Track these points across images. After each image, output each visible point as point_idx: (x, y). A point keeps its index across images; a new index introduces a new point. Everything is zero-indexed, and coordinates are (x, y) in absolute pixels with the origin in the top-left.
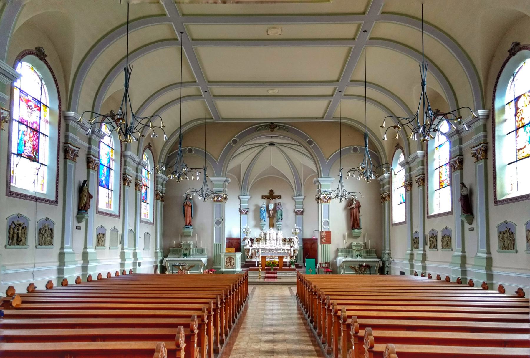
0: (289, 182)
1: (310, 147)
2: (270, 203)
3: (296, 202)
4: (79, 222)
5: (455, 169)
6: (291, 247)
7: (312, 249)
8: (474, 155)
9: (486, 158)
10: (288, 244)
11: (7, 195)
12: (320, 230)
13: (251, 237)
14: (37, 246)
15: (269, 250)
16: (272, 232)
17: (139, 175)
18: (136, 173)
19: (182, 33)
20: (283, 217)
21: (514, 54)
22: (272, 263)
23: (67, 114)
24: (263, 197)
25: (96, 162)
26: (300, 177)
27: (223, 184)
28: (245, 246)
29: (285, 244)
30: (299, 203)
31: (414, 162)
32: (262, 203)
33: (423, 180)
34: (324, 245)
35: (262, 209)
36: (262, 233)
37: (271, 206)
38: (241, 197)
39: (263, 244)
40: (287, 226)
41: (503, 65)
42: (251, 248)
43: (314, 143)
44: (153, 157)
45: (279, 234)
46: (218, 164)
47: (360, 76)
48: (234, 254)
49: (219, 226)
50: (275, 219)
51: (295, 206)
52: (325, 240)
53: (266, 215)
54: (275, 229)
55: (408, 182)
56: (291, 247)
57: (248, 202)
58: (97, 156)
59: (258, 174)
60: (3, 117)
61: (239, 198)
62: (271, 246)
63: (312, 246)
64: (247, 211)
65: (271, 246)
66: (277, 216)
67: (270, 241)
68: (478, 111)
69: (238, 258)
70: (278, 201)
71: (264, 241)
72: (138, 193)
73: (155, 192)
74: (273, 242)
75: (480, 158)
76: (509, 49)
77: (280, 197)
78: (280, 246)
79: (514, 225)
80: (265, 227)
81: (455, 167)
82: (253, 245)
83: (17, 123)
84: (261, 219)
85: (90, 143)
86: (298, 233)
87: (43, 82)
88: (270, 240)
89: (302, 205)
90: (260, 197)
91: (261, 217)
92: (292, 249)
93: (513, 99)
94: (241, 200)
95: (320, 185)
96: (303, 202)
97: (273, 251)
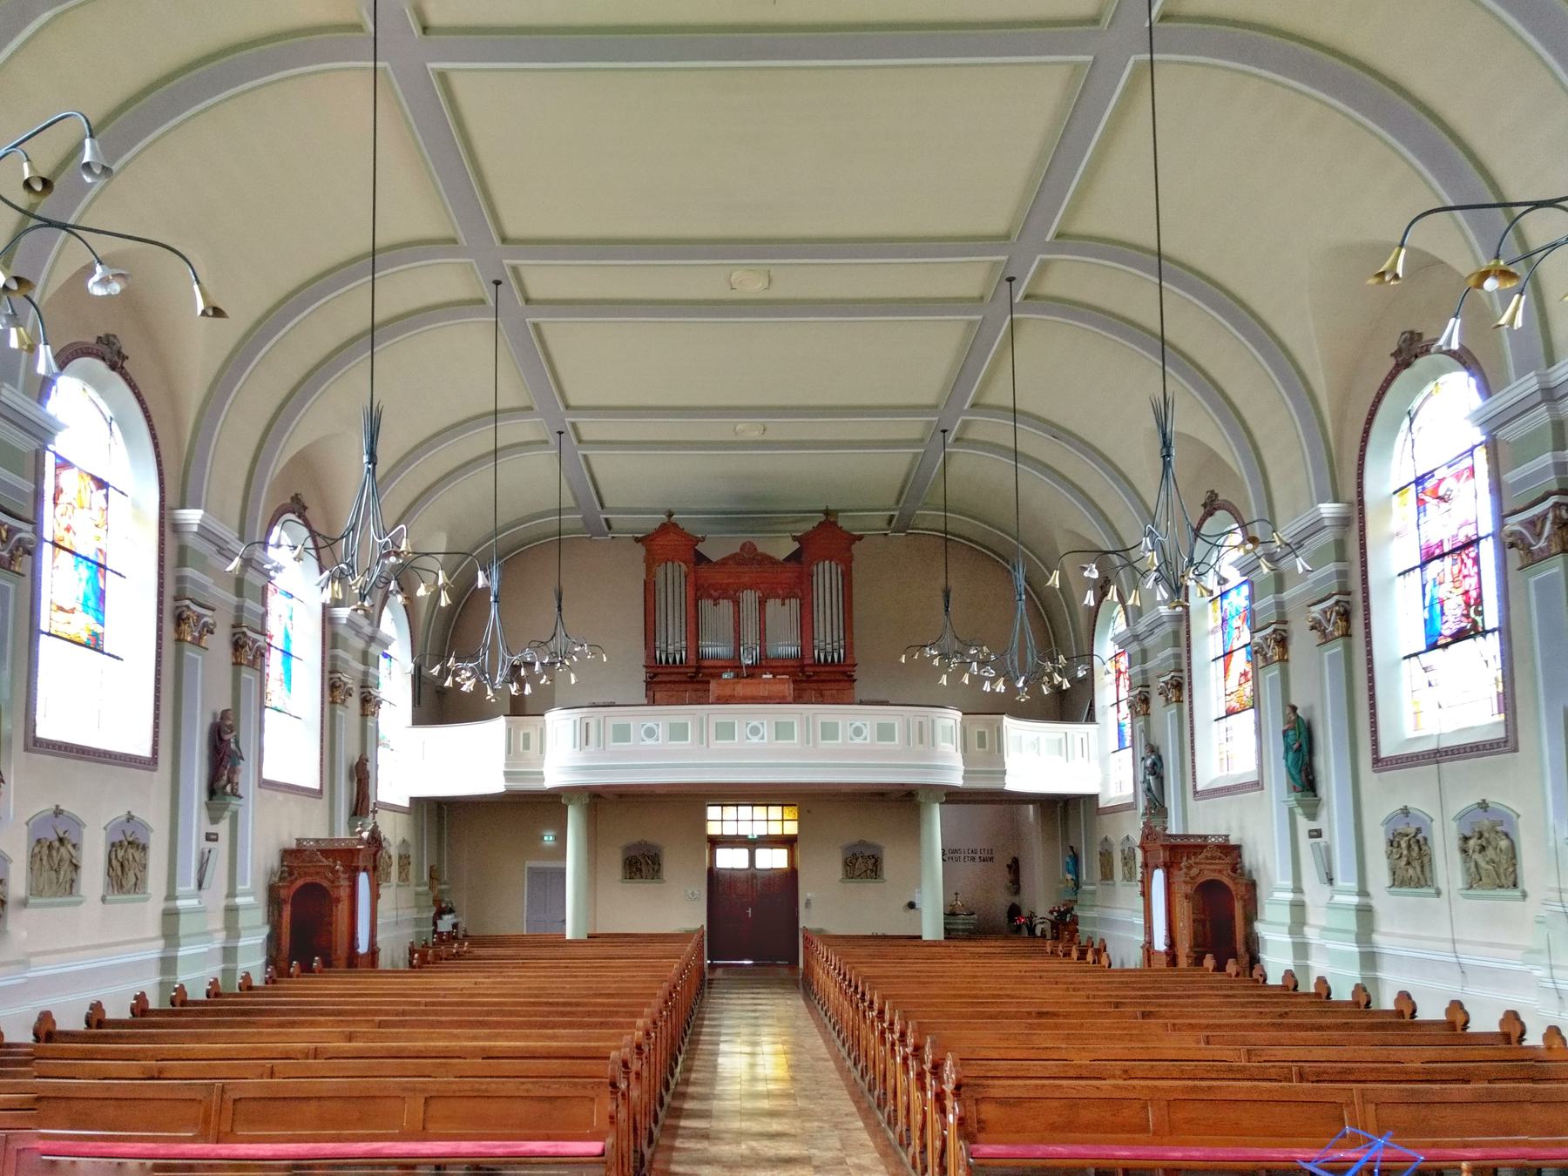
4: (214, 820)
5: (1268, 662)
8: (1316, 626)
9: (1347, 634)
11: (26, 749)
17: (246, 604)
18: (234, 600)
19: (497, 283)
21: (1408, 365)
23: (184, 517)
25: (205, 619)
31: (1153, 637)
33: (1179, 687)
41: (1378, 393)
44: (148, 418)
47: (999, 395)
55: (1137, 692)
58: (259, 629)
60: (20, 540)
68: (1321, 505)
72: (339, 712)
73: (327, 675)
75: (1332, 632)
76: (1395, 348)
79: (1426, 818)
81: (1266, 654)
83: (51, 546)
85: (239, 593)
87: (114, 425)
93: (1413, 479)
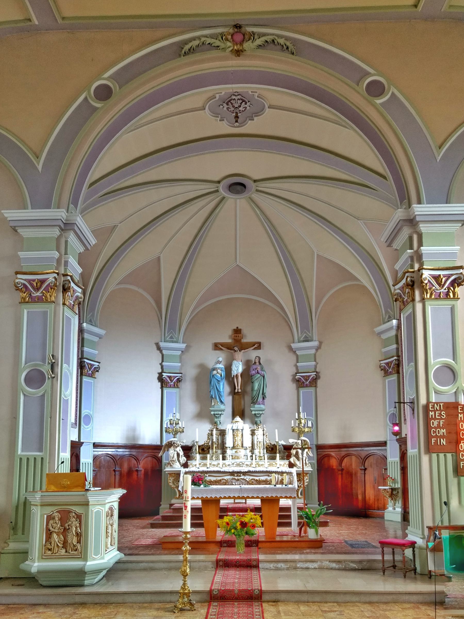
0: (279, 310)
1: (374, 106)
2: (233, 359)
3: (297, 356)
6: (291, 465)
7: (342, 470)
10: (282, 458)
12: (423, 401)
13: (187, 442)
14: (290, 463)
15: (232, 473)
16: (240, 428)
20: (268, 391)
22: (239, 527)
24: (217, 347)
26: (309, 294)
27: (58, 239)
28: (169, 464)
29: (274, 458)
30: (307, 358)
32: (215, 361)
34: (442, 455)
35: (215, 372)
36: (215, 432)
37: (238, 367)
38: (162, 344)
39: (217, 459)
40: (276, 414)
42: (183, 470)
43: (392, 88)
45: (259, 433)
46: (40, 167)
48: (81, 499)
49: (40, 392)
50: (248, 399)
51: (297, 367)
52: (443, 437)
53: (224, 388)
54: (248, 420)
56: (291, 465)
57: (181, 359)
59: (206, 289)
61: (159, 348)
62: (238, 465)
63: (343, 464)
64: (179, 380)
65: (238, 465)
66: (253, 389)
67: (234, 451)
69: (98, 513)
70: (253, 354)
71: (219, 451)
74: (242, 452)
77: (258, 346)
78: (261, 463)
80: (222, 418)
82: (189, 462)
84: (212, 397)
86: (306, 430)
88: (234, 448)
89: (314, 363)
90: (210, 346)
91: (212, 393)
92: (294, 471)
94: (164, 352)
95: (415, 237)
96: (315, 355)
97: (242, 477)
